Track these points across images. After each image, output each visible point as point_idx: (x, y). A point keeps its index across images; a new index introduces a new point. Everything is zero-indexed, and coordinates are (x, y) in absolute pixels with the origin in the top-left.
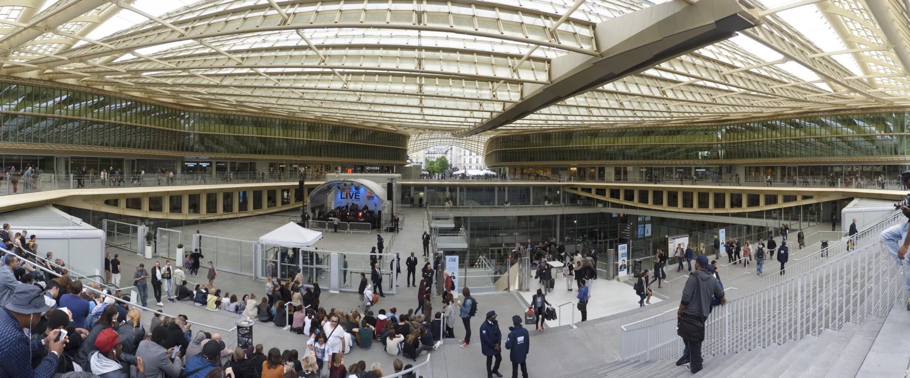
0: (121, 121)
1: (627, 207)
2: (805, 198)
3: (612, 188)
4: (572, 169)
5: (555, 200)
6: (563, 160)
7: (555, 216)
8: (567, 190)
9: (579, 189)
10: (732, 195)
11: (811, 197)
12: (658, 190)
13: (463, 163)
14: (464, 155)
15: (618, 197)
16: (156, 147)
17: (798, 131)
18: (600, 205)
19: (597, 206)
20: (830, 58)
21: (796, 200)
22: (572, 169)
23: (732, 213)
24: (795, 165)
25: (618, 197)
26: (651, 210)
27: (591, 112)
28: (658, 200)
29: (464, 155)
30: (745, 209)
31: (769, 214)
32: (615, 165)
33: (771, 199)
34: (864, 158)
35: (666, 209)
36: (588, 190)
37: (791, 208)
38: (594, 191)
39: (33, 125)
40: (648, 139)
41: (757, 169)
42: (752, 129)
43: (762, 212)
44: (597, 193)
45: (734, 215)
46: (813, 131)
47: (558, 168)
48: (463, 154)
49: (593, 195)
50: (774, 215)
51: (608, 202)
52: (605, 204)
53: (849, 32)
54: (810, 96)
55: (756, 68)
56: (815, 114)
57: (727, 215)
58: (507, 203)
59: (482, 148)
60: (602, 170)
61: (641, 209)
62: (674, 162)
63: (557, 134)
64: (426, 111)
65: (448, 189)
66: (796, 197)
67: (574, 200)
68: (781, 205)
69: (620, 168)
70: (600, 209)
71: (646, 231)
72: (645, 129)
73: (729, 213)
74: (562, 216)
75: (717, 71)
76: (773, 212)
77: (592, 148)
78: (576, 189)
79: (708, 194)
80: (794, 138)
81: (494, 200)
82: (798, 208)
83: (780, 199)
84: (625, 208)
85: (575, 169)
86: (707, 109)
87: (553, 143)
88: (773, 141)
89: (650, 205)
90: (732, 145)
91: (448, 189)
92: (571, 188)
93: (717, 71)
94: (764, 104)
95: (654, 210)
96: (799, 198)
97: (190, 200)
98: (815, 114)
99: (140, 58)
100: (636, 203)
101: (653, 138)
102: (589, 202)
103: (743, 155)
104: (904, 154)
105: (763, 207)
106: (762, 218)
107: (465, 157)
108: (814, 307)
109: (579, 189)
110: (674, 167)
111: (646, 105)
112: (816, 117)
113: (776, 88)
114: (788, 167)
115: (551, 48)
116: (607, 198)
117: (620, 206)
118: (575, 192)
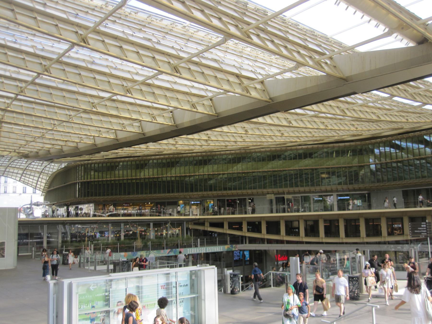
0: (94, 178)
3: (268, 220)
8: (191, 227)
9: (207, 224)
15: (259, 231)
25: (259, 231)
26: (322, 243)
32: (218, 196)
36: (220, 225)
38: (226, 226)
39: (227, 179)
40: (173, 171)
51: (246, 237)
55: (372, 103)
56: (417, 134)
59: (43, 182)
60: (306, 199)
61: (288, 242)
65: (152, 224)
75: (338, 107)
86: (244, 138)
91: (152, 224)
92: (195, 224)
93: (338, 107)
98: (417, 134)
99: (188, 140)
101: (210, 167)
109: (207, 224)
112: (418, 137)
113: (414, 118)
116: (245, 233)
118: (201, 228)
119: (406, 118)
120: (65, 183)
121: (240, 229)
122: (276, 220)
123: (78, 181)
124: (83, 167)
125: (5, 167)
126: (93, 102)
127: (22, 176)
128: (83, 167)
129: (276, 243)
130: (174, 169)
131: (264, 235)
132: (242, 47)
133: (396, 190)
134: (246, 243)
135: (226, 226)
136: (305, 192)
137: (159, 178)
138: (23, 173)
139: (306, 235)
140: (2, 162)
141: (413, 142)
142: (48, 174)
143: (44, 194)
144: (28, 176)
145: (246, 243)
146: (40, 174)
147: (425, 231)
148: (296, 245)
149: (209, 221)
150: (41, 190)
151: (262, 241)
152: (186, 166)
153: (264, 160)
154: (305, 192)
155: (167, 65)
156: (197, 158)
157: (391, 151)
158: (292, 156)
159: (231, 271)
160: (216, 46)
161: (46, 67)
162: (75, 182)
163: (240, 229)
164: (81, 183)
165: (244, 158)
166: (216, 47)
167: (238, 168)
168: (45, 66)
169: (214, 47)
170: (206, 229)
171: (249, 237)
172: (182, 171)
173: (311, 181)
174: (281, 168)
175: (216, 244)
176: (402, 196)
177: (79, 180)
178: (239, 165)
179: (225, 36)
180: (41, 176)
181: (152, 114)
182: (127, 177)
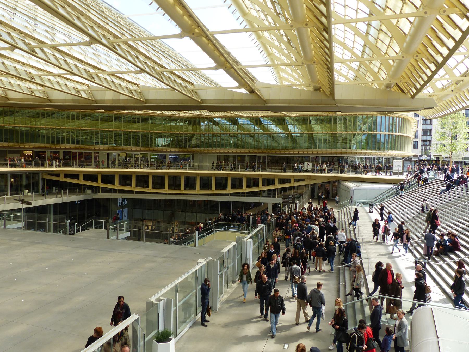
1: (105, 191)
9: (62, 175)
11: (303, 180)
12: (270, 177)
16: (393, 149)
20: (214, 37)
21: (290, 182)
22: (26, 152)
23: (136, 191)
30: (245, 189)
33: (269, 181)
36: (76, 176)
38: (81, 177)
41: (226, 159)
43: (243, 193)
44: (103, 182)
45: (248, 194)
49: (81, 181)
51: (99, 187)
52: (95, 190)
53: (247, 11)
54: (193, 79)
57: (242, 194)
63: (394, 136)
66: (290, 180)
69: (90, 153)
71: (124, 215)
73: (134, 191)
79: (115, 175)
81: (61, 193)
85: (31, 152)
92: (49, 175)
94: (73, 67)
96: (292, 181)
104: (346, 148)
105: (261, 188)
106: (244, 196)
108: (416, 242)
116: (99, 184)
121: (96, 180)
122: (130, 174)
129: (173, 187)
131: (117, 186)
132: (351, 226)
135: (81, 177)
136: (145, 151)
139: (153, 187)
141: (371, 326)
145: (99, 193)
147: (413, 94)
148: (144, 195)
149: (10, 173)
151: (115, 191)
153: (102, 120)
154: (145, 151)
159: (69, 221)
163: (96, 180)
170: (61, 180)
171: (102, 188)
173: (148, 139)
175: (76, 192)
176: (114, 99)
179: (91, 39)
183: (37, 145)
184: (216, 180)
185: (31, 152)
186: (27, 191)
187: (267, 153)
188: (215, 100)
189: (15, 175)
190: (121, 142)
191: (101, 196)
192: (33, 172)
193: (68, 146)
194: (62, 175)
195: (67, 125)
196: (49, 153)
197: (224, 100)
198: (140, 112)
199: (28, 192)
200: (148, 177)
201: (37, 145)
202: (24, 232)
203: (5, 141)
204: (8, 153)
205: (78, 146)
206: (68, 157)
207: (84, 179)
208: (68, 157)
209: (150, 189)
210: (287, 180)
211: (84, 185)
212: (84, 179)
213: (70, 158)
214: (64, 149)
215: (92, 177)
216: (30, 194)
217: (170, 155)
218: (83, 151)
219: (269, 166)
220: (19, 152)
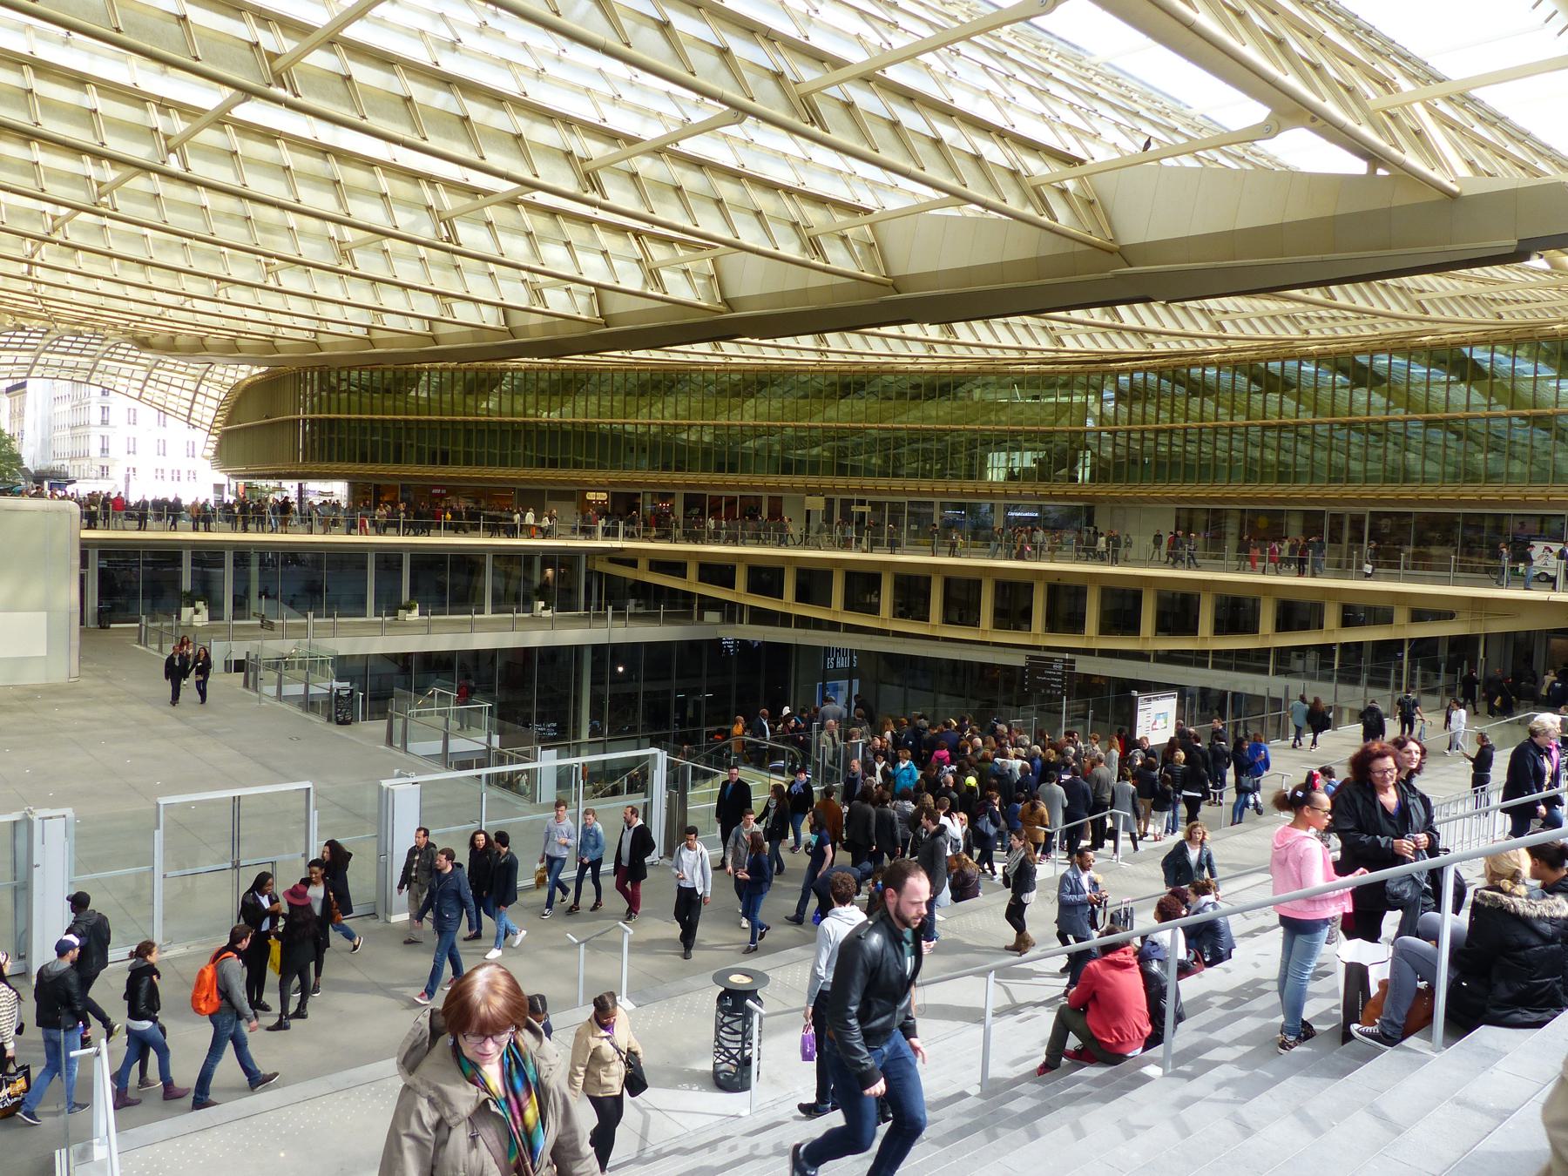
1: (804, 622)
2: (1350, 617)
4: (591, 496)
5: (563, 599)
6: (445, 462)
7: (578, 649)
9: (643, 564)
10: (948, 583)
13: (95, 451)
14: (104, 423)
17: (1361, 395)
18: (712, 616)
19: (701, 617)
22: (591, 496)
24: (1355, 510)
27: (541, 298)
28: (1065, 614)
29: (104, 423)
31: (1284, 660)
33: (1294, 613)
34: (1525, 491)
35: (1040, 643)
36: (675, 567)
37: (1359, 645)
38: (692, 572)
41: (1216, 520)
42: (1199, 389)
43: (1263, 654)
44: (702, 579)
45: (1225, 660)
46: (1325, 395)
47: (542, 492)
48: (95, 416)
49: (690, 584)
50: (1298, 665)
52: (731, 612)
58: (409, 608)
59: (207, 411)
61: (850, 628)
62: (940, 486)
64: (39, 273)
67: (653, 601)
68: (1333, 634)
69: (758, 499)
70: (711, 627)
72: (835, 378)
74: (597, 649)
76: (1294, 654)
77: (629, 428)
78: (633, 563)
80: (1275, 421)
81: (692, 614)
82: (1394, 646)
83: (1332, 617)
84: (1216, 666)
85: (603, 496)
87: (708, 430)
88: (1319, 428)
89: (885, 618)
90: (1163, 439)
92: (613, 561)
95: (897, 634)
96: (1401, 616)
97: (593, 654)
100: (836, 611)
102: (681, 605)
103: (1168, 468)
105: (1268, 637)
107: (104, 431)
109: (643, 564)
110: (937, 500)
111: (598, 261)
114: (1333, 516)
115: (706, 100)
116: (739, 594)
117: (784, 620)
119: (1496, 308)
120: (267, 417)
121: (730, 584)
123: (302, 415)
124: (316, 374)
125: (32, 354)
126: (274, 49)
127: (145, 384)
128: (316, 374)
130: (671, 400)
131: (787, 603)
133: (1160, 506)
134: (741, 622)
137: (1303, 425)
138: (148, 378)
139: (947, 620)
140: (6, 339)
142: (157, 381)
143: (215, 438)
144: (177, 391)
145: (741, 622)
146: (200, 383)
150: (203, 426)
152: (642, 395)
155: (769, 86)
156: (1291, 365)
157: (1295, 403)
158: (895, 388)
160: (974, 34)
161: (278, 64)
162: (296, 417)
163: (730, 584)
164: (312, 420)
165: (860, 386)
166: (975, 39)
167: (748, 414)
168: (273, 57)
169: (967, 38)
170: (640, 578)
172: (593, 407)
174: (860, 422)
175: (362, 603)
177: (305, 413)
178: (845, 405)
180: (202, 389)
181: (582, 160)
182: (1468, 410)
183: (625, 476)
184: (1218, 608)
185: (603, 496)
186: (542, 604)
187: (904, 492)
188: (760, 296)
189: (506, 558)
190: (943, 469)
191: (733, 633)
192: (330, 549)
193: (704, 478)
194: (643, 564)
195: (904, 418)
196: (648, 497)
197: (806, 290)
198: (657, 355)
199: (543, 609)
200: (977, 584)
201: (625, 476)
202: (298, 712)
203: (678, 469)
204: (549, 499)
205: (731, 478)
206: (696, 511)
207: (702, 579)
208: (696, 511)
209: (935, 624)
210: (1377, 612)
211: (701, 596)
212: (702, 579)
213: (702, 514)
214: (942, 494)
215: (718, 572)
216: (548, 613)
217: (943, 506)
218: (737, 494)
219: (1243, 548)
220: (573, 495)
